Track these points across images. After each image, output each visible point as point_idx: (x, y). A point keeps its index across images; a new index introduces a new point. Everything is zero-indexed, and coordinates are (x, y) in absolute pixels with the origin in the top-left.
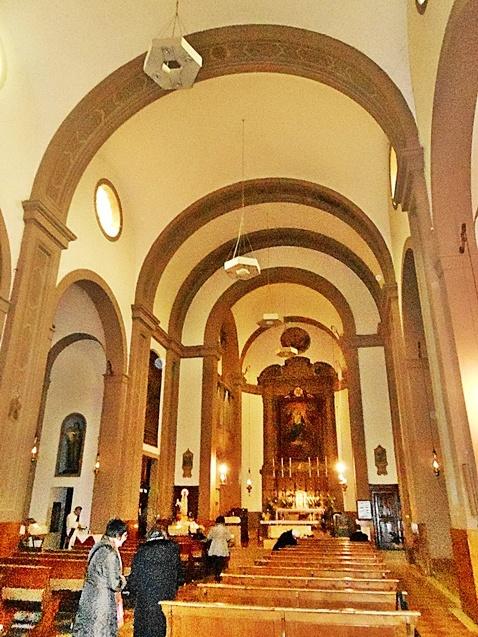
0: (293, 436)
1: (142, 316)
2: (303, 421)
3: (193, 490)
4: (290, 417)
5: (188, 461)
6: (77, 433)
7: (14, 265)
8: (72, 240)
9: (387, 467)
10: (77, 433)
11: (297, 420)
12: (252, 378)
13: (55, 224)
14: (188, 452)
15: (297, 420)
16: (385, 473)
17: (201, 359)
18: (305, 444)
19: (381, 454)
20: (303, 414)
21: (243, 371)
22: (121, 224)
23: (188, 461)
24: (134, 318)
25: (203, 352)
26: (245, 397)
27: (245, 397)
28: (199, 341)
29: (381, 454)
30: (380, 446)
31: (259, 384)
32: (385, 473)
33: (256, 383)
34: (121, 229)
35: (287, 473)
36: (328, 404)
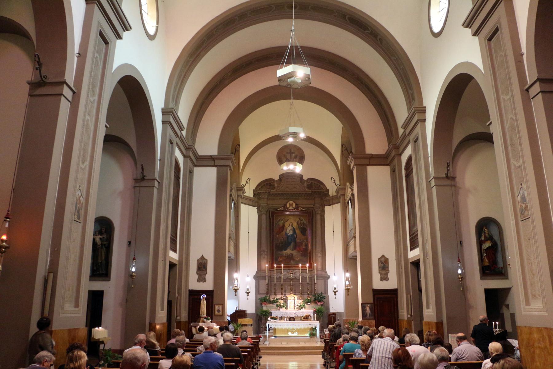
0: (285, 246)
1: (172, 120)
2: (294, 230)
3: (210, 294)
4: (283, 228)
5: (202, 267)
6: (105, 236)
7: (76, 50)
8: (127, 30)
9: (389, 274)
10: (105, 236)
11: (289, 231)
12: (249, 192)
13: (423, 107)
14: (203, 258)
15: (289, 231)
16: (204, 280)
17: (214, 170)
18: (295, 253)
19: (384, 264)
20: (295, 225)
21: (243, 183)
22: (158, 23)
23: (202, 267)
24: (163, 122)
25: (217, 163)
26: (244, 208)
27: (244, 208)
28: (213, 151)
29: (384, 264)
30: (383, 256)
31: (254, 196)
32: (204, 280)
33: (252, 195)
34: (157, 27)
35: (279, 279)
36: (318, 217)
